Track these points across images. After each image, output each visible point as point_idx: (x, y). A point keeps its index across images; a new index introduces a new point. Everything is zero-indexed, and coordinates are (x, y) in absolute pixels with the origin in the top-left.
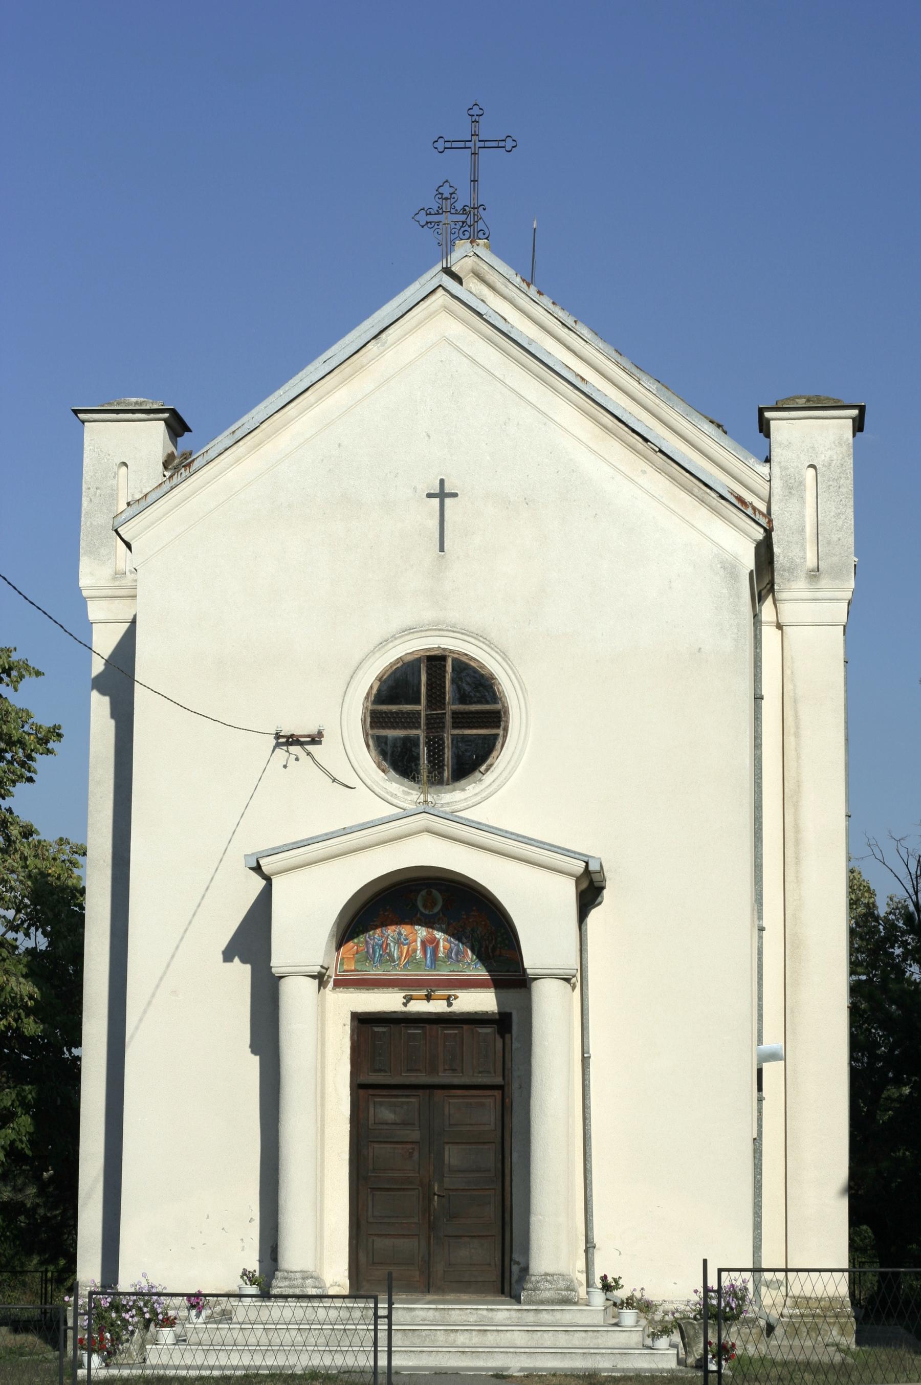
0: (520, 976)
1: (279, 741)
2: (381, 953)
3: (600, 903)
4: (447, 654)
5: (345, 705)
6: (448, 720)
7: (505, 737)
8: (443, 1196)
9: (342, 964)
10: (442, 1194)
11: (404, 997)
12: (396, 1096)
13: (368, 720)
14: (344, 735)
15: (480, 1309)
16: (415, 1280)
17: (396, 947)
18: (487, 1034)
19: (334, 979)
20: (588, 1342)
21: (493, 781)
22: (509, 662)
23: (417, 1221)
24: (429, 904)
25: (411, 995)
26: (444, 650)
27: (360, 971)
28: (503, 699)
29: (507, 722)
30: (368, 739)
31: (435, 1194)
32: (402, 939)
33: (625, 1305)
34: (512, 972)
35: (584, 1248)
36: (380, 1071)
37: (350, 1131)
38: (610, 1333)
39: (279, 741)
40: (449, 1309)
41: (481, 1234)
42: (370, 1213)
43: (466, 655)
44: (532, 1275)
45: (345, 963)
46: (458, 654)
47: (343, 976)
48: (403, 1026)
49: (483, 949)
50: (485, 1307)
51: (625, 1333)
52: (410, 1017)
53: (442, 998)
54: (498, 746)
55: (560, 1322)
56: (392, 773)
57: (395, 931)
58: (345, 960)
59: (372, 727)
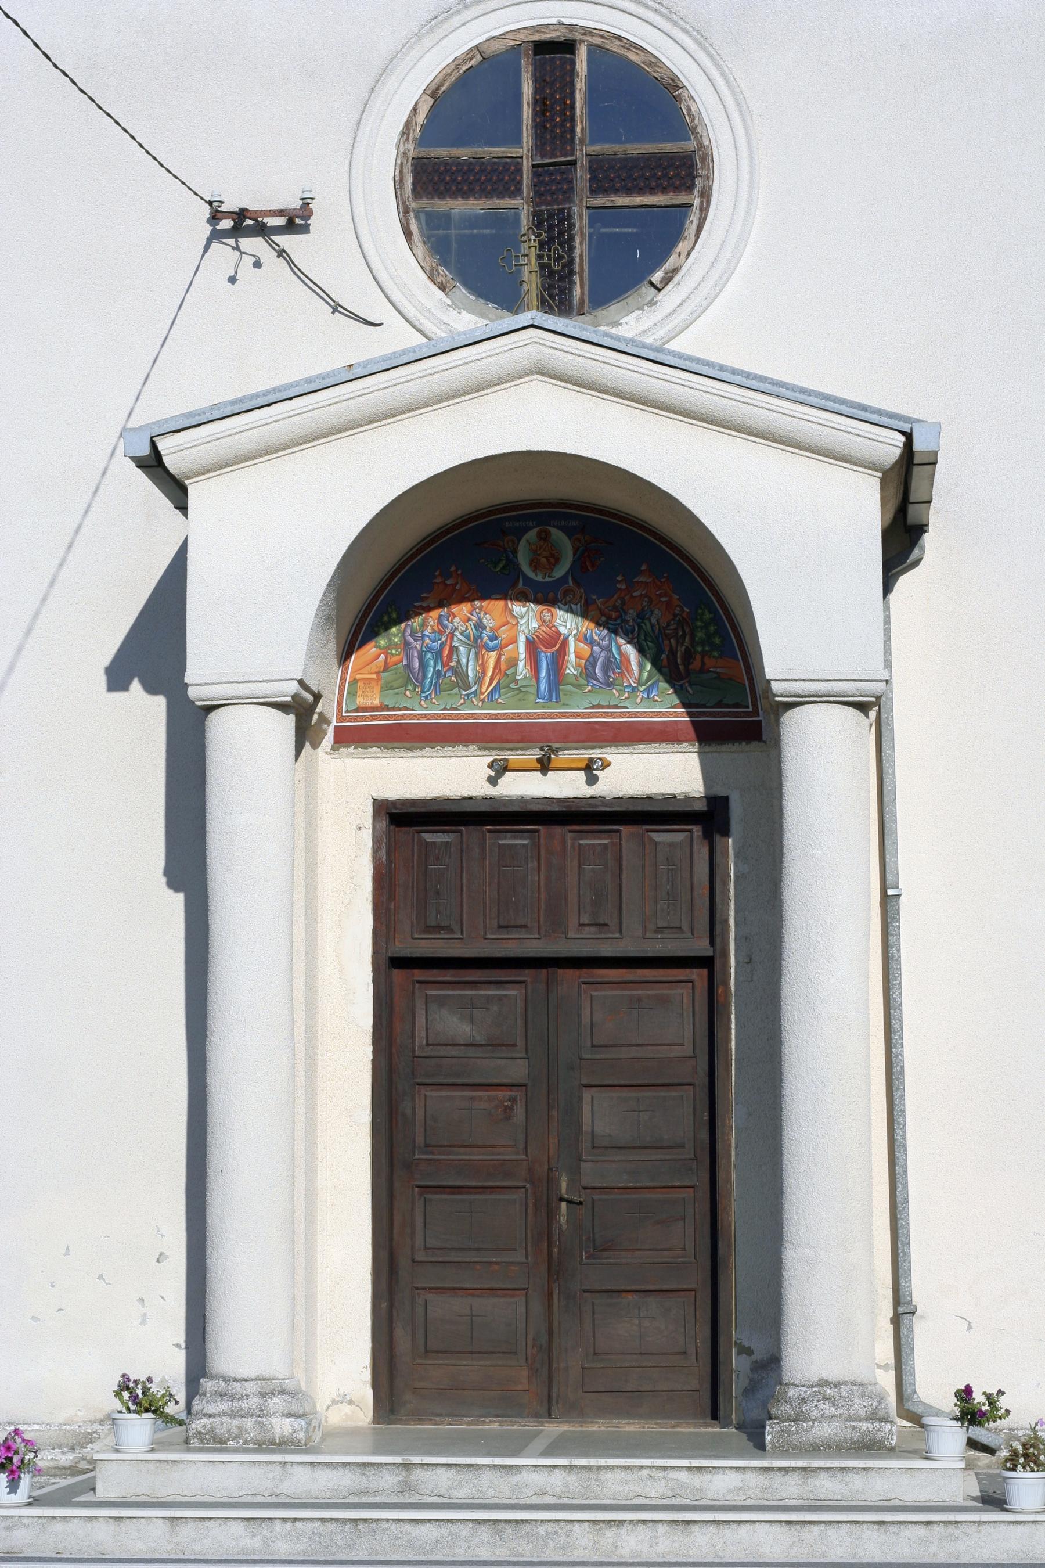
0: (748, 714)
1: (218, 227)
2: (439, 667)
3: (917, 563)
4: (578, 37)
5: (360, 149)
6: (582, 175)
7: (704, 209)
8: (581, 1203)
9: (353, 694)
10: (577, 1199)
11: (491, 766)
12: (474, 984)
13: (409, 180)
14: (356, 212)
15: (673, 1468)
16: (520, 1387)
17: (472, 656)
18: (671, 845)
19: (335, 726)
20: (933, 1549)
21: (681, 304)
22: (711, 49)
23: (524, 1259)
24: (544, 560)
25: (506, 760)
26: (572, 28)
27: (393, 709)
28: (699, 130)
29: (708, 178)
30: (407, 220)
31: (562, 1199)
32: (485, 638)
33: (1022, 1460)
34: (728, 706)
35: (891, 1315)
36: (438, 928)
37: (373, 1061)
38: (986, 1527)
39: (218, 227)
40: (599, 1467)
41: (665, 1287)
42: (419, 1241)
43: (619, 38)
44: (788, 1385)
45: (359, 692)
46: (602, 37)
47: (355, 719)
48: (489, 831)
49: (664, 656)
50: (685, 1463)
51: (1020, 1527)
52: (502, 809)
53: (574, 765)
54: (691, 230)
55: (863, 1497)
56: (461, 291)
57: (469, 620)
58: (360, 684)
59: (416, 193)
